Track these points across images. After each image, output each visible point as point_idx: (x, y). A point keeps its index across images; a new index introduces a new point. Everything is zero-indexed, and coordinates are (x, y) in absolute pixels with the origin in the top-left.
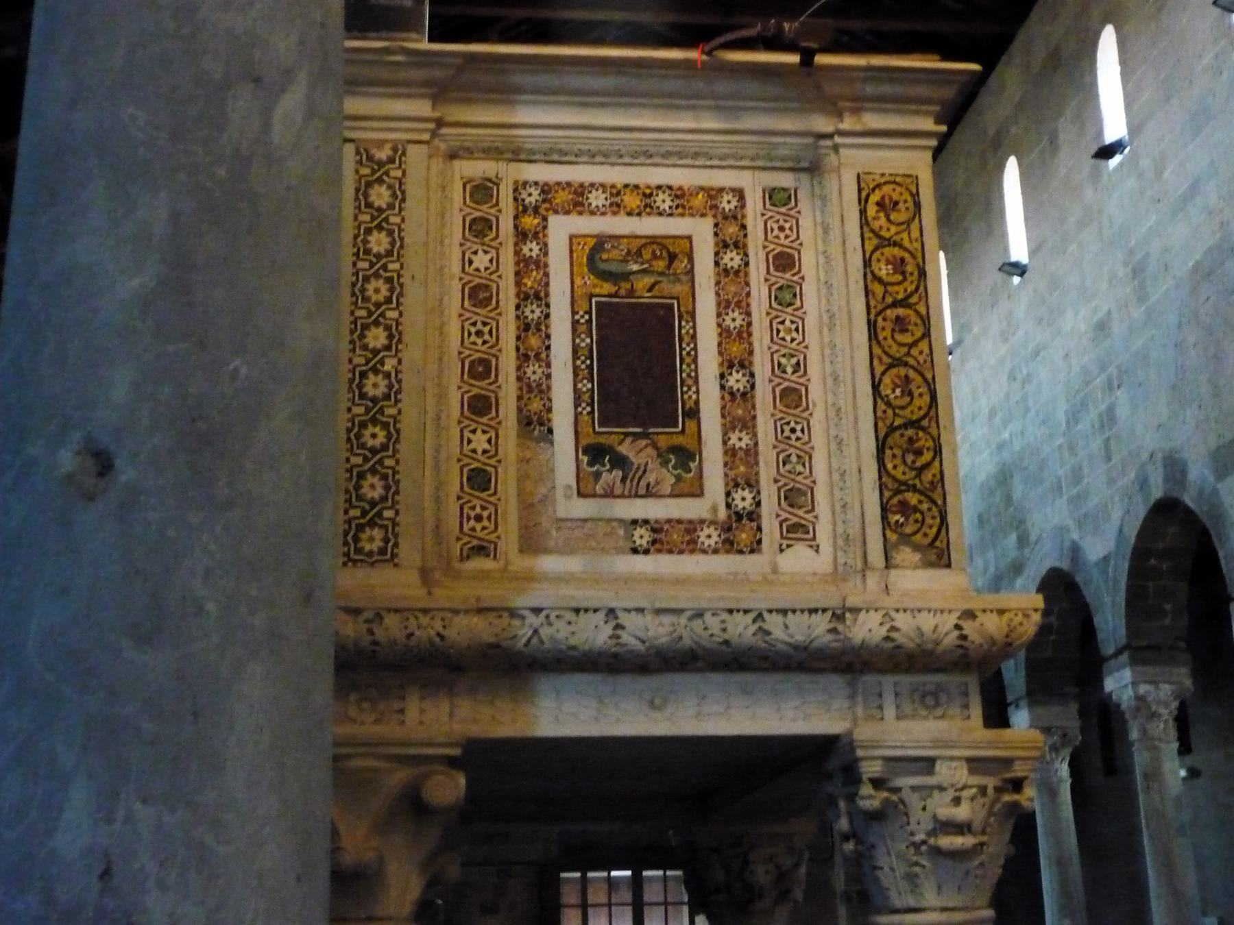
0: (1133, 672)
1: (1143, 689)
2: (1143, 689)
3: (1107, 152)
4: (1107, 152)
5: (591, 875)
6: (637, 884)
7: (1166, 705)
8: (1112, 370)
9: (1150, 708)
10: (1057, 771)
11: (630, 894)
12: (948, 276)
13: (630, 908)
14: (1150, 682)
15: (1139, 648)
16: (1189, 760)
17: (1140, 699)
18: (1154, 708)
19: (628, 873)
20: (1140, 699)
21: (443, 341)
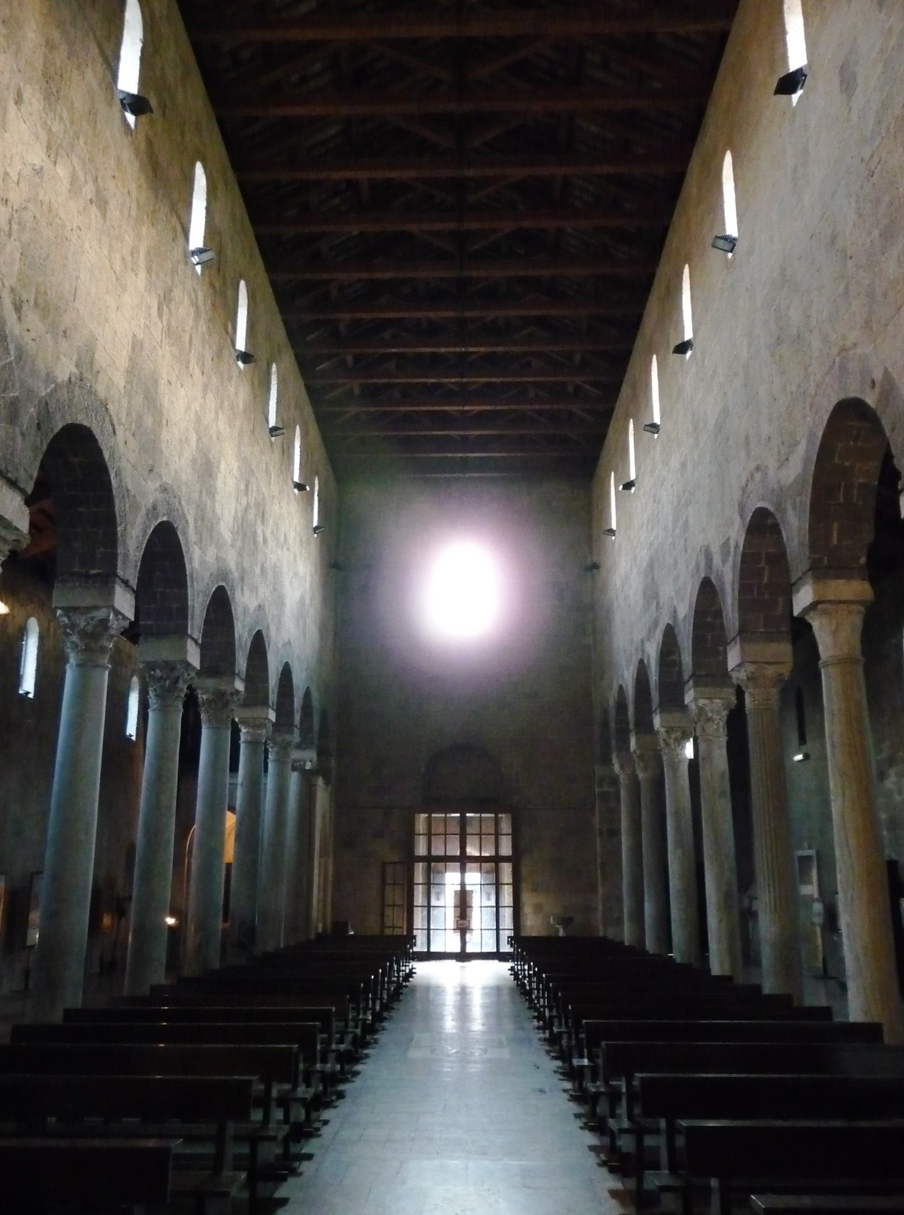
0: (695, 692)
1: (702, 702)
2: (702, 702)
3: (682, 348)
4: (682, 348)
5: (433, 815)
6: (463, 822)
7: (718, 713)
8: (687, 494)
9: (706, 715)
10: (678, 755)
11: (459, 828)
12: (634, 434)
13: (458, 836)
14: (707, 698)
15: (700, 676)
16: (804, 748)
17: (701, 709)
18: (710, 715)
19: (458, 815)
20: (701, 709)
21: (121, 481)
